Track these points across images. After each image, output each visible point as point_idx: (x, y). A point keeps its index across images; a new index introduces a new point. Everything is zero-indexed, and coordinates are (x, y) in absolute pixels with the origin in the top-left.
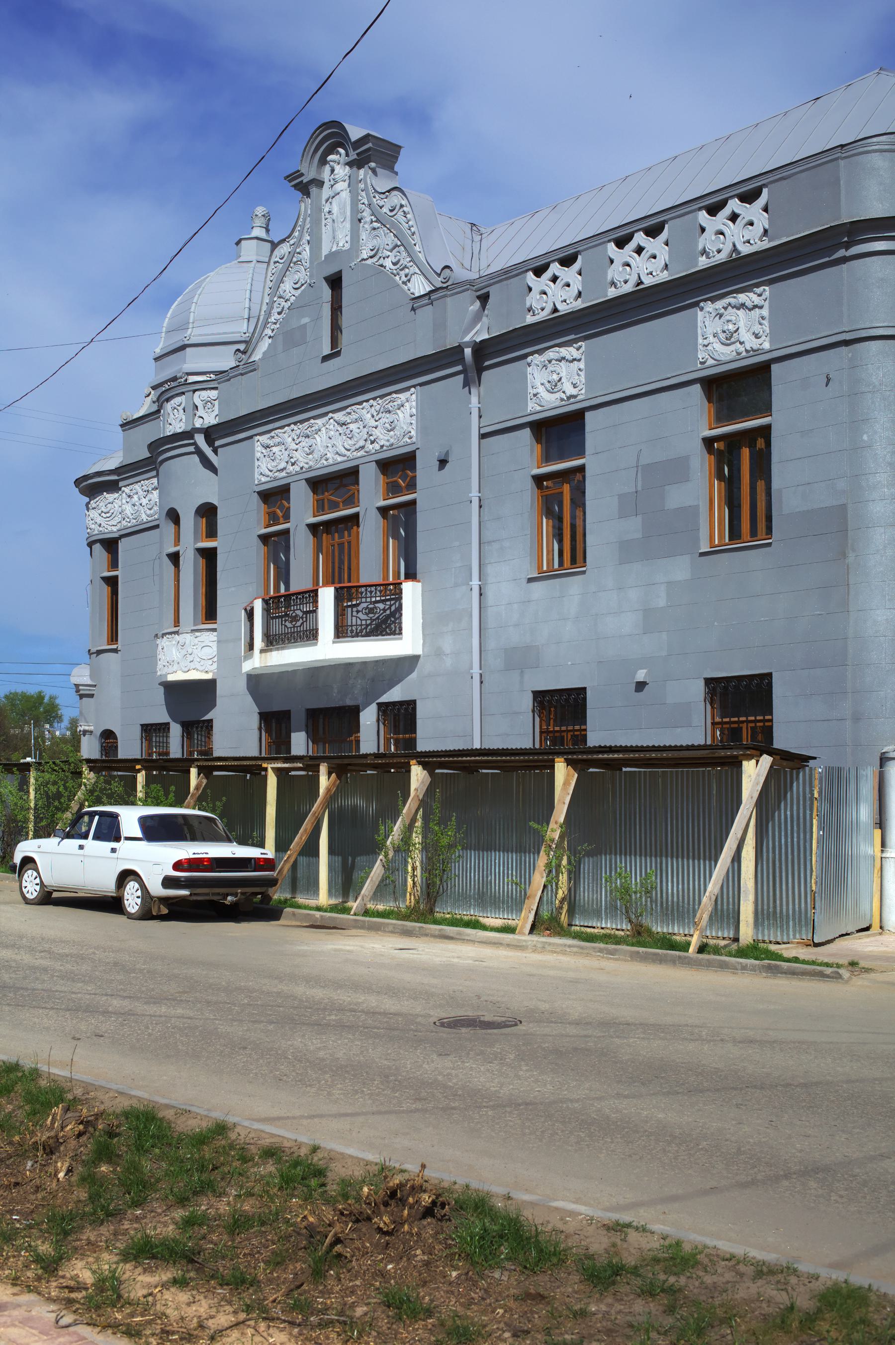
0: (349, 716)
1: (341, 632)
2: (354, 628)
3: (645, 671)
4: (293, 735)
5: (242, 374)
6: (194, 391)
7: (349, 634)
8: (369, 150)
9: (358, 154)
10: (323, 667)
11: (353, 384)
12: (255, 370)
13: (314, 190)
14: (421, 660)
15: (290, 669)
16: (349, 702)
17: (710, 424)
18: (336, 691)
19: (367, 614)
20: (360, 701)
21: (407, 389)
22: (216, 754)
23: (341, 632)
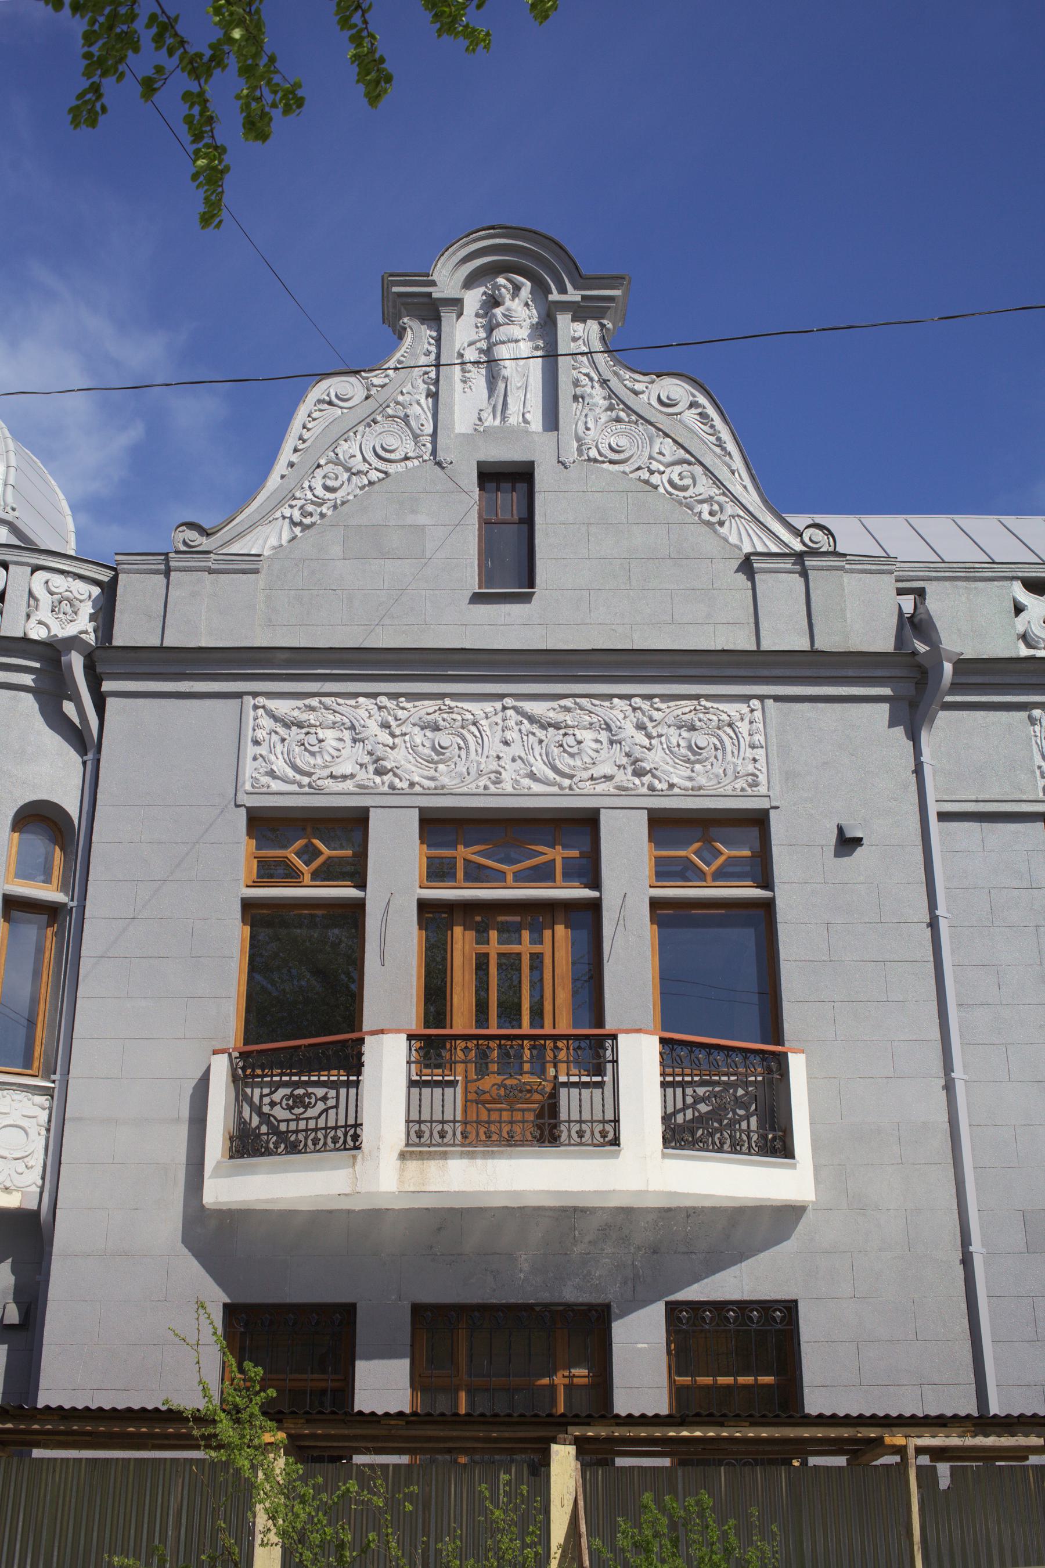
0: (588, 1329)
1: (679, 1135)
2: (320, 1135)
3: (10, 1260)
4: (361, 1366)
5: (211, 571)
6: (35, 569)
7: (331, 1145)
8: (611, 299)
9: (583, 297)
10: (482, 1210)
11: (677, 658)
12: (256, 571)
13: (447, 317)
14: (809, 1215)
15: (707, 1204)
16: (571, 1294)
17: (421, 881)
18: (526, 1267)
19: (290, 1108)
20: (611, 1294)
21: (746, 698)
22: (621, 1407)
23: (679, 1135)
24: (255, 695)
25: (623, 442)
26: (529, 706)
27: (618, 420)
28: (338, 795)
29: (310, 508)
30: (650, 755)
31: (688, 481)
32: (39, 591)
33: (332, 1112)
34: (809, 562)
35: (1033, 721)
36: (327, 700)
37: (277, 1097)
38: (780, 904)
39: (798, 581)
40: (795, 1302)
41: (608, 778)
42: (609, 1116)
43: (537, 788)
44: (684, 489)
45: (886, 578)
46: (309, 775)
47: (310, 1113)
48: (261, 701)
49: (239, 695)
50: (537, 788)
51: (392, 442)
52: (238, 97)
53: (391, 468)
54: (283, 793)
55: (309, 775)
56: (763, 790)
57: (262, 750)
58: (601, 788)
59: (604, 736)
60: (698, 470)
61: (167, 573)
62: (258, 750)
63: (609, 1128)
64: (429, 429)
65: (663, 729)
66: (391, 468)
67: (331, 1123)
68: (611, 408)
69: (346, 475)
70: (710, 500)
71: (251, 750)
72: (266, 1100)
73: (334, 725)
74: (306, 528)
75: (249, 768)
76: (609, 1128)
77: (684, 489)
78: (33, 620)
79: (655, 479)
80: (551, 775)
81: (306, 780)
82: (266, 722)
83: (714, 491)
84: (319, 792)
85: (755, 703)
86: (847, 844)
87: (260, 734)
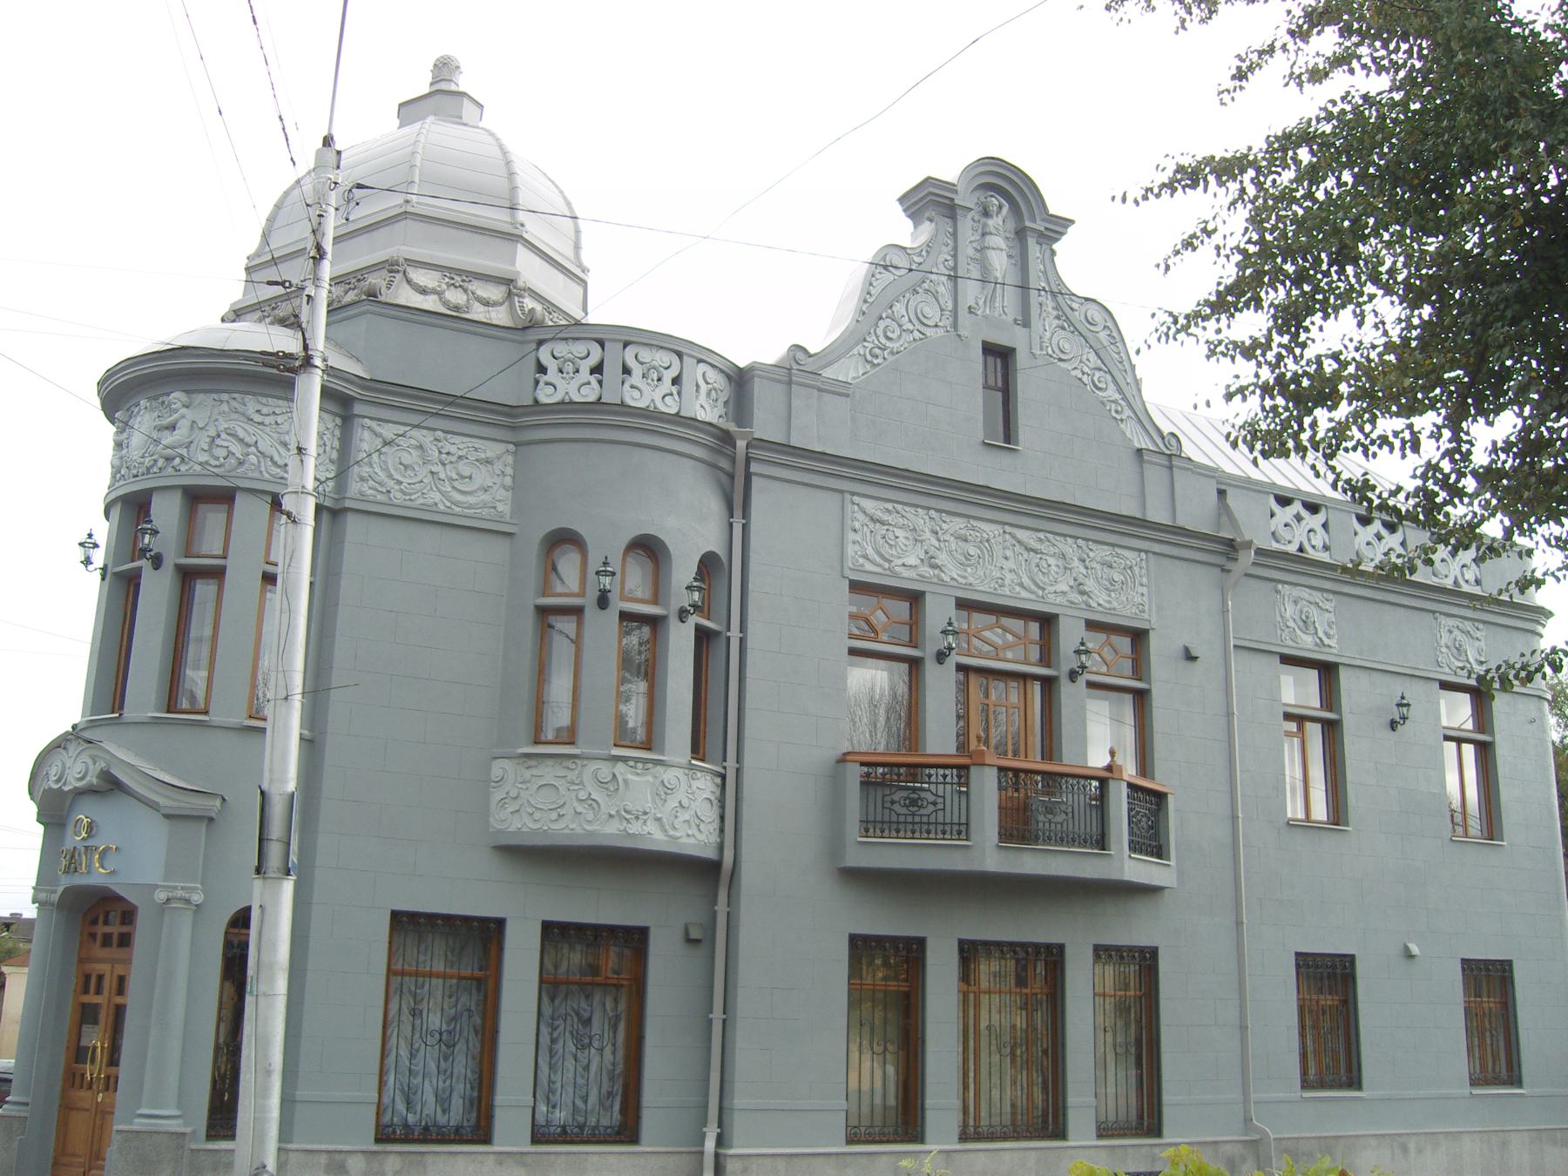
24: (853, 494)
25: (1067, 347)
26: (1020, 534)
27: (1063, 328)
28: (907, 578)
29: (877, 351)
30: (1086, 581)
31: (1102, 385)
32: (631, 363)
33: (940, 813)
34: (1175, 462)
35: (1278, 592)
36: (899, 507)
37: (896, 797)
38: (1155, 693)
39: (1165, 472)
40: (1510, 962)
41: (1064, 593)
42: (963, 820)
43: (1024, 594)
44: (1100, 389)
45: (301, 260)
46: (890, 561)
47: (922, 811)
48: (856, 499)
49: (842, 492)
50: (1024, 594)
51: (928, 311)
52: (1250, 149)
53: (928, 332)
54: (872, 572)
55: (890, 561)
56: (1146, 616)
57: (858, 537)
58: (1059, 600)
59: (1060, 563)
60: (1108, 377)
61: (790, 383)
62: (858, 537)
63: (963, 828)
64: (950, 306)
65: (1094, 565)
66: (928, 332)
67: (940, 820)
68: (1058, 317)
69: (898, 332)
70: (1115, 402)
71: (851, 536)
72: (888, 799)
73: (1054, 555)
74: (874, 365)
75: (851, 550)
76: (963, 828)
77: (1100, 389)
78: (627, 386)
79: (1085, 378)
80: (878, 559)
81: (886, 565)
82: (860, 516)
83: (1117, 396)
84: (896, 576)
85: (1143, 555)
86: (1190, 657)
87: (857, 525)
